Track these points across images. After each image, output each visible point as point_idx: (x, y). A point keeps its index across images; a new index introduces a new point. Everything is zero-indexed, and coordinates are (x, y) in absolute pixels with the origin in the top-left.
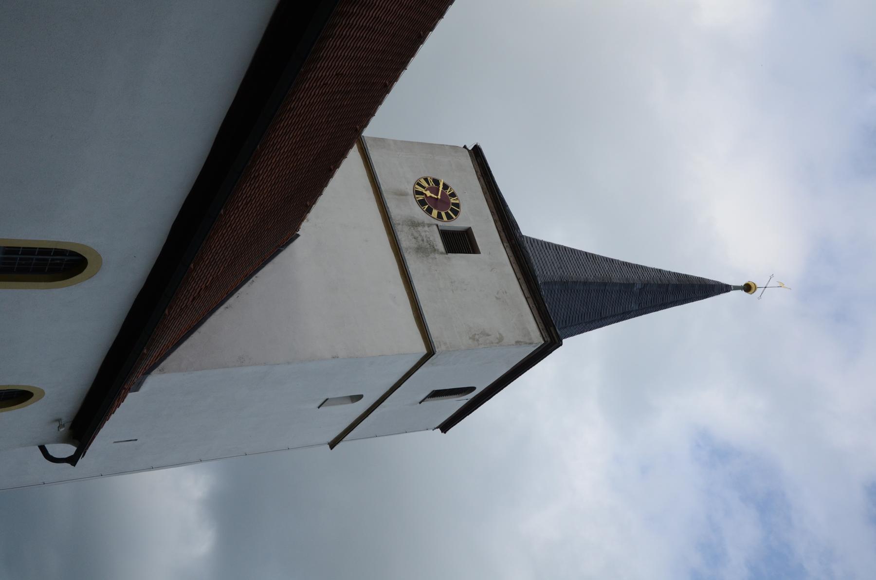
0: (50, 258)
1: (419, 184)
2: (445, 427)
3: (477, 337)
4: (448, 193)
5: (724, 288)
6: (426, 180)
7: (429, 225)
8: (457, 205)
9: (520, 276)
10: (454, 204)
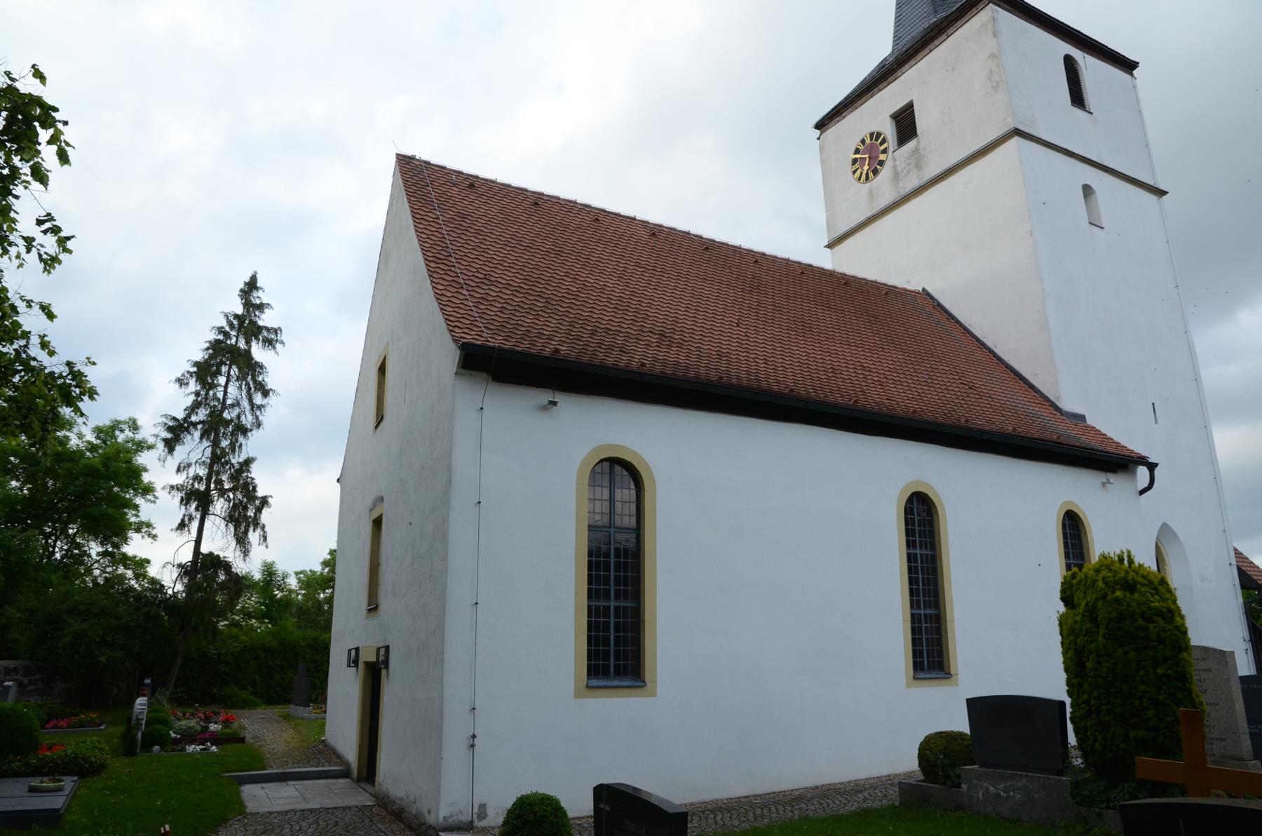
2: (1128, 65)
6: (854, 172)
7: (895, 160)
8: (871, 135)
9: (926, 50)
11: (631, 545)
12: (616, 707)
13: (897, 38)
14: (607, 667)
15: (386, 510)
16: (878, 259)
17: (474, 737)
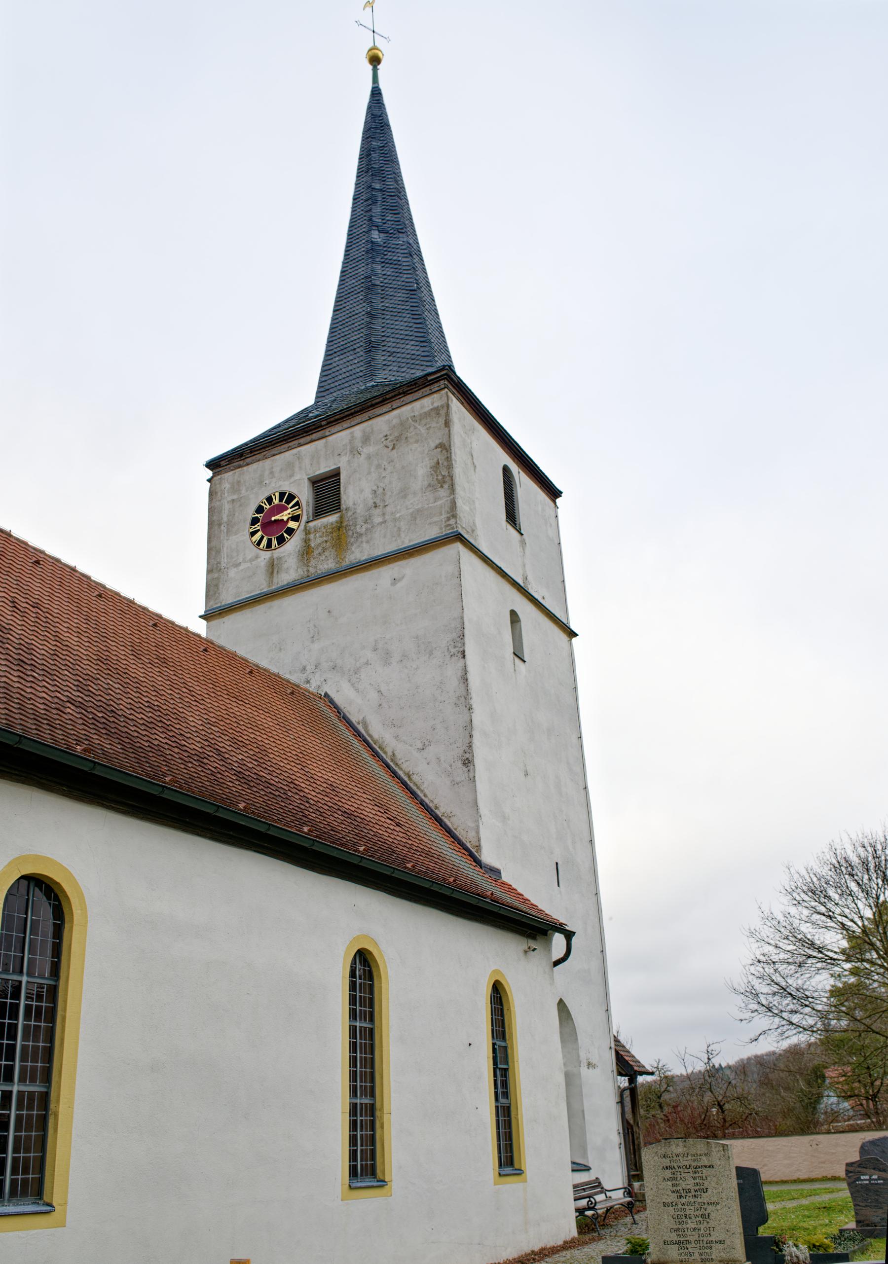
0: (358, 981)
1: (259, 543)
2: (554, 493)
3: (440, 477)
4: (268, 507)
5: (376, 94)
6: (253, 534)
7: (307, 532)
8: (282, 495)
9: (365, 416)
10: (281, 500)
13: (322, 390)
16: (279, 642)
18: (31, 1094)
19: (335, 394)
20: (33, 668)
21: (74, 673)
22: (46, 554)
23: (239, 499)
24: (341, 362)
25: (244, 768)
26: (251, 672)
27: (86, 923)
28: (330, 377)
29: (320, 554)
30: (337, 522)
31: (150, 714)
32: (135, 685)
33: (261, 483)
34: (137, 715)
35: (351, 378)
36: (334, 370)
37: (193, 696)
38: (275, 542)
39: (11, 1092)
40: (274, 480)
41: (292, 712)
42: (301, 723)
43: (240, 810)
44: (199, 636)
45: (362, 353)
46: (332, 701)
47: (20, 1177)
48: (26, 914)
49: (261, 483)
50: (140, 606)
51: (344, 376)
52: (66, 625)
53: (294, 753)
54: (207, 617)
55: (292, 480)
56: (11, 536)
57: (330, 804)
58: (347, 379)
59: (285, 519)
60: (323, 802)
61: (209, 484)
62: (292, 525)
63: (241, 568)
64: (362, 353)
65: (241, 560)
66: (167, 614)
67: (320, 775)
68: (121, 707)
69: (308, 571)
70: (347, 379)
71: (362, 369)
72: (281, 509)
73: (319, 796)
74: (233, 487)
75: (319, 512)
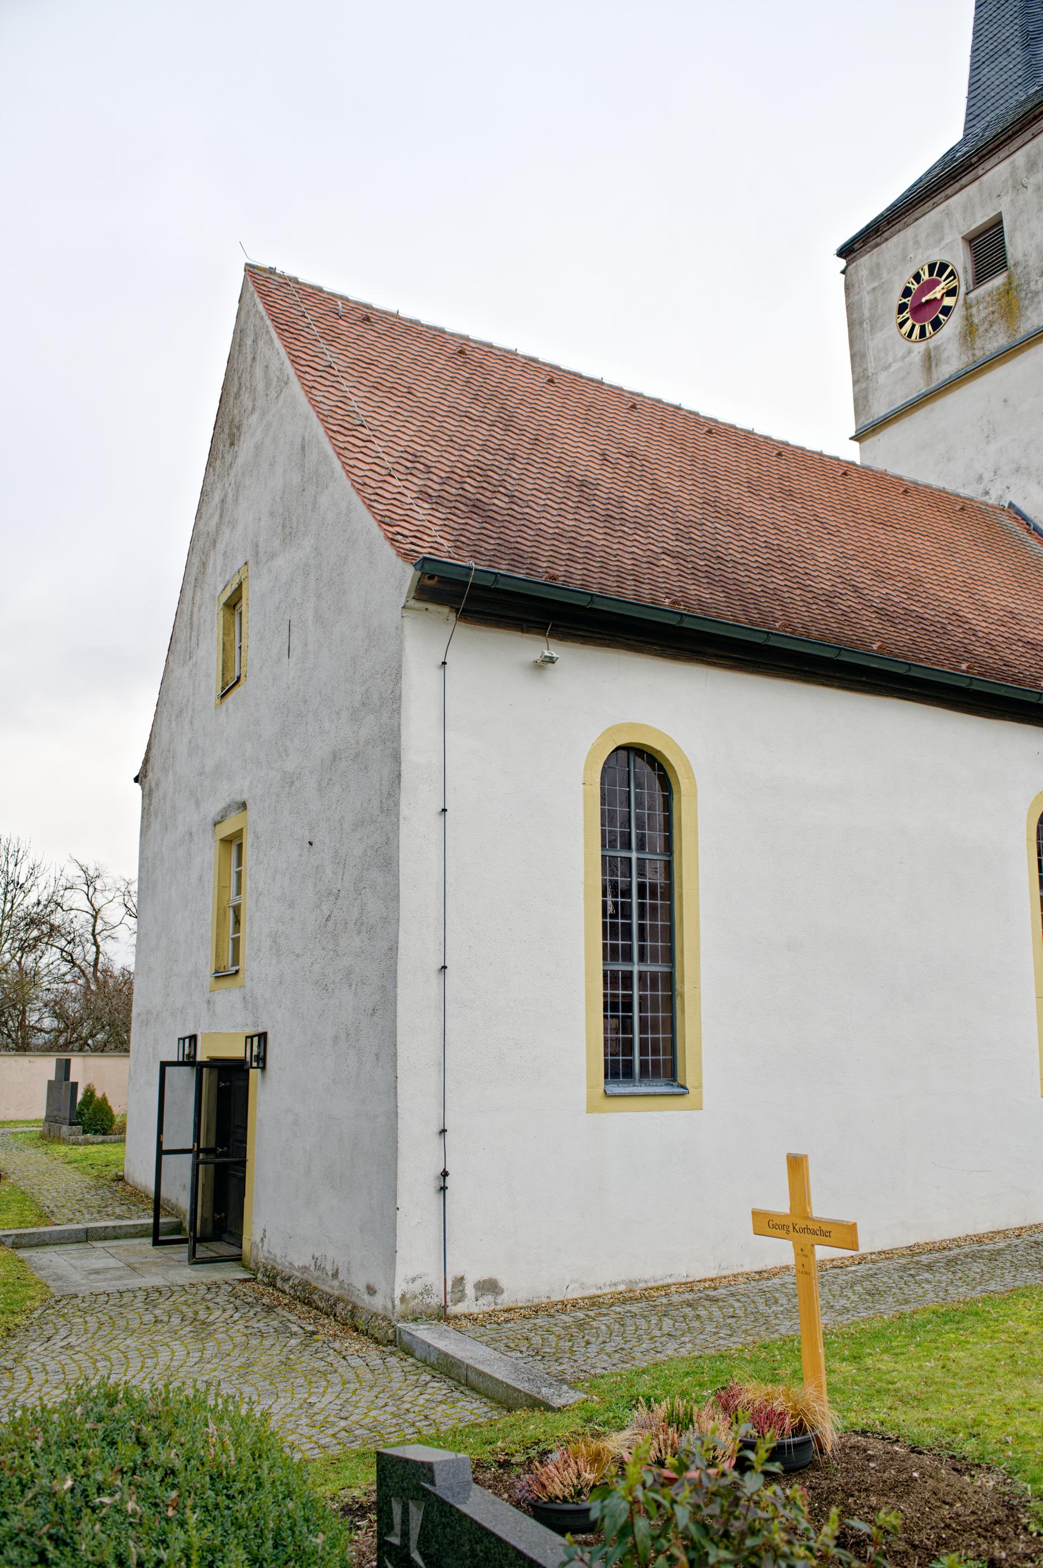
1: (910, 335)
4: (916, 286)
6: (901, 325)
7: (967, 306)
8: (931, 267)
10: (931, 274)
11: (660, 880)
12: (645, 1122)
13: (972, 117)
14: (629, 1065)
15: (256, 825)
17: (445, 1174)
18: (654, 975)
19: (988, 119)
20: (623, 522)
21: (673, 521)
22: (644, 397)
23: (881, 286)
24: (993, 73)
25: (889, 603)
26: (906, 491)
27: (696, 792)
28: (979, 97)
29: (987, 331)
30: (1004, 285)
31: (768, 555)
32: (750, 525)
33: (905, 258)
34: (750, 558)
35: (1007, 90)
36: (983, 87)
37: (825, 528)
38: (929, 329)
39: (631, 972)
40: (920, 251)
41: (960, 531)
42: (972, 543)
43: (964, 672)
44: (854, 464)
45: (1018, 52)
46: (1018, 512)
47: (650, 1058)
48: (629, 787)
49: (905, 258)
50: (761, 436)
51: (997, 90)
52: (665, 470)
53: (961, 579)
54: (858, 438)
55: (943, 244)
56: (603, 384)
57: (1007, 635)
58: (1002, 94)
59: (939, 296)
60: (997, 633)
61: (843, 276)
62: (948, 301)
63: (892, 369)
64: (1018, 52)
65: (891, 360)
66: (795, 440)
67: (995, 601)
68: (731, 551)
69: (974, 355)
70: (1002, 94)
71: (1020, 73)
72: (932, 285)
73: (992, 626)
74: (871, 273)
75: (981, 277)
